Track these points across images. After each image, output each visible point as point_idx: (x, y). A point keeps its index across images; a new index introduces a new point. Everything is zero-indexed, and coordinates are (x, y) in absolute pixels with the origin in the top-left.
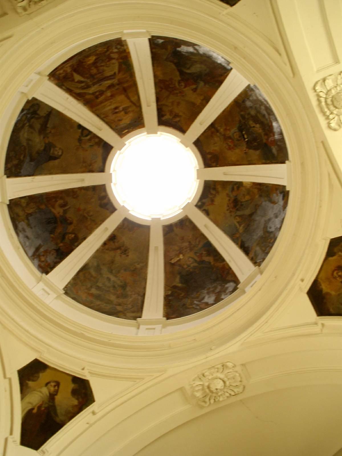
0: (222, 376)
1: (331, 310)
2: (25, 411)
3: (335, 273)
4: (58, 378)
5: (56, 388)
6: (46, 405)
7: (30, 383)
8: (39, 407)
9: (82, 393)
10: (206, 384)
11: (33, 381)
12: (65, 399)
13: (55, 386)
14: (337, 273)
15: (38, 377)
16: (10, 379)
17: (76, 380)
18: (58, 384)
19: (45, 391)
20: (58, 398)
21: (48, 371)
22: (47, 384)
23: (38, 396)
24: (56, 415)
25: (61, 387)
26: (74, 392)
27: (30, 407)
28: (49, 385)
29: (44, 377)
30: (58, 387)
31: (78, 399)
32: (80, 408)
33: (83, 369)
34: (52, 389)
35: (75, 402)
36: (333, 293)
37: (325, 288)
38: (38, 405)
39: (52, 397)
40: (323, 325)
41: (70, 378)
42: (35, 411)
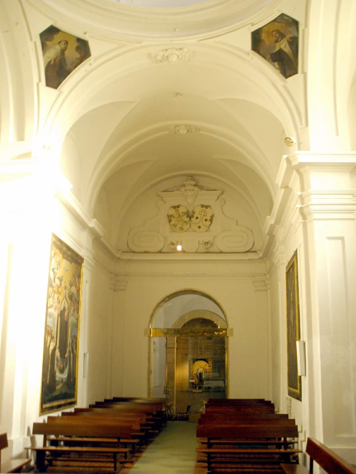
0: (178, 54)
1: (261, 52)
2: (46, 65)
3: (274, 33)
4: (67, 39)
5: (66, 45)
6: (59, 58)
7: (48, 43)
8: (55, 60)
9: (83, 49)
10: (166, 55)
11: (50, 41)
12: (71, 54)
13: (65, 44)
14: (275, 34)
15: (53, 38)
16: (35, 43)
17: (79, 40)
18: (67, 43)
19: (58, 48)
20: (67, 53)
21: (60, 33)
22: (59, 43)
23: (53, 52)
24: (66, 65)
25: (69, 44)
26: (78, 49)
27: (49, 60)
28: (61, 43)
29: (57, 38)
30: (67, 45)
31: (80, 53)
32: (81, 60)
33: (85, 33)
34: (63, 46)
35: (78, 55)
36: (267, 43)
37: (264, 36)
38: (54, 58)
39: (63, 51)
40: (252, 58)
41: (76, 39)
42: (52, 62)
